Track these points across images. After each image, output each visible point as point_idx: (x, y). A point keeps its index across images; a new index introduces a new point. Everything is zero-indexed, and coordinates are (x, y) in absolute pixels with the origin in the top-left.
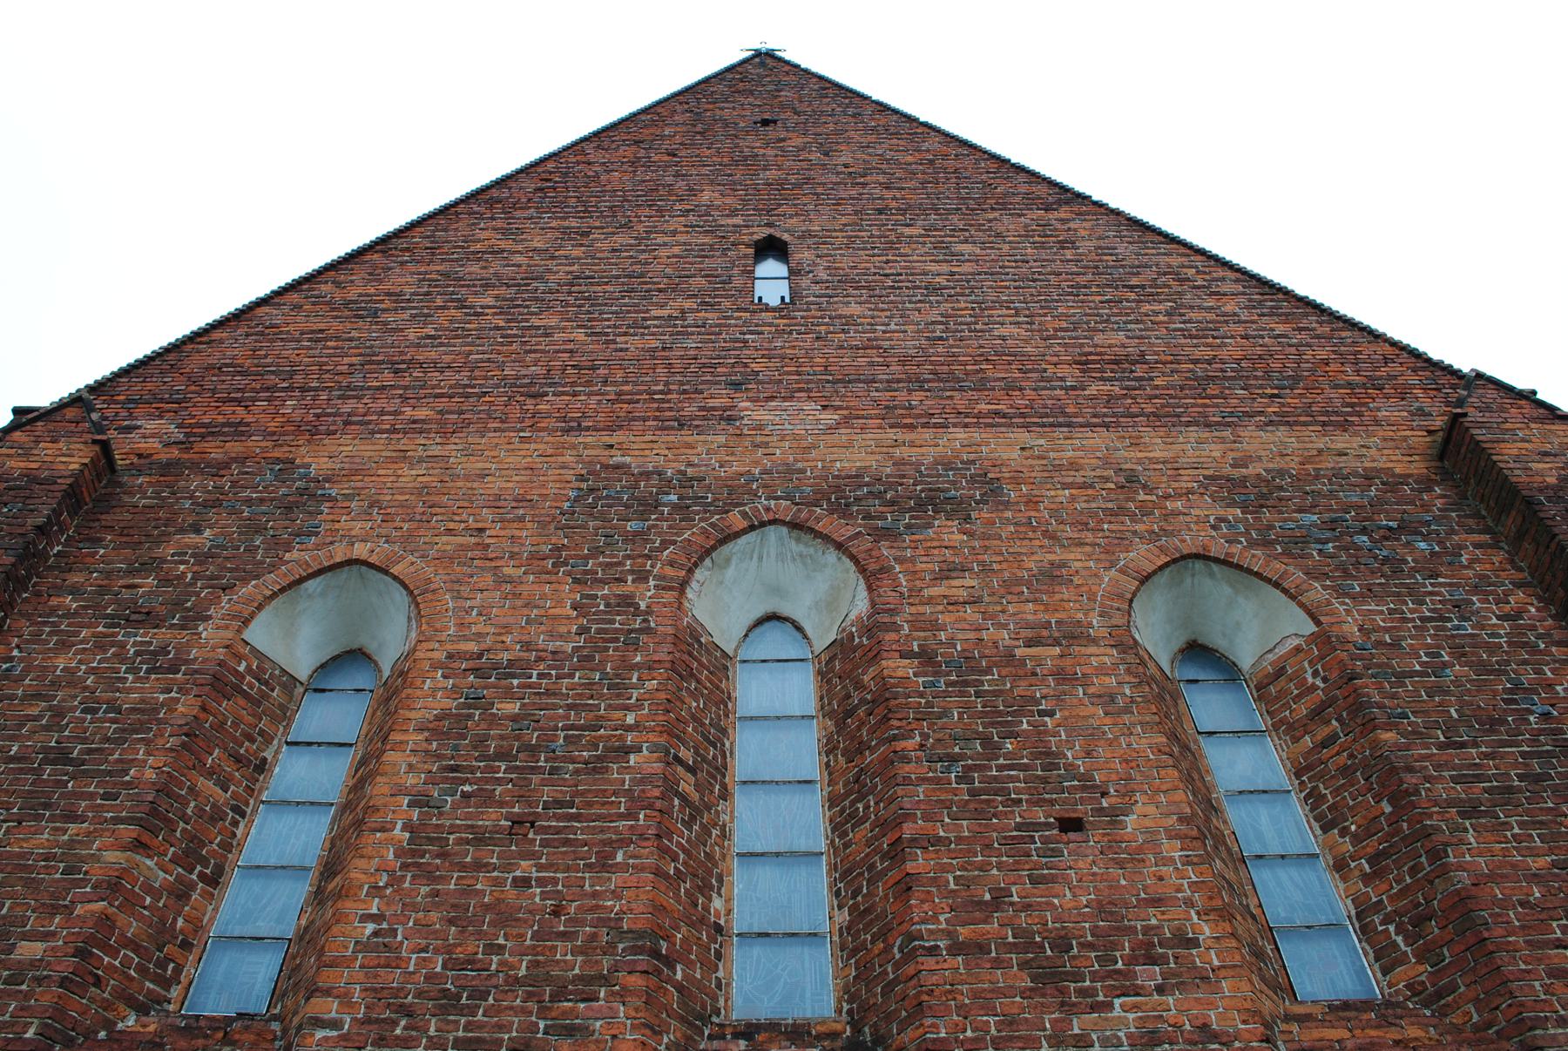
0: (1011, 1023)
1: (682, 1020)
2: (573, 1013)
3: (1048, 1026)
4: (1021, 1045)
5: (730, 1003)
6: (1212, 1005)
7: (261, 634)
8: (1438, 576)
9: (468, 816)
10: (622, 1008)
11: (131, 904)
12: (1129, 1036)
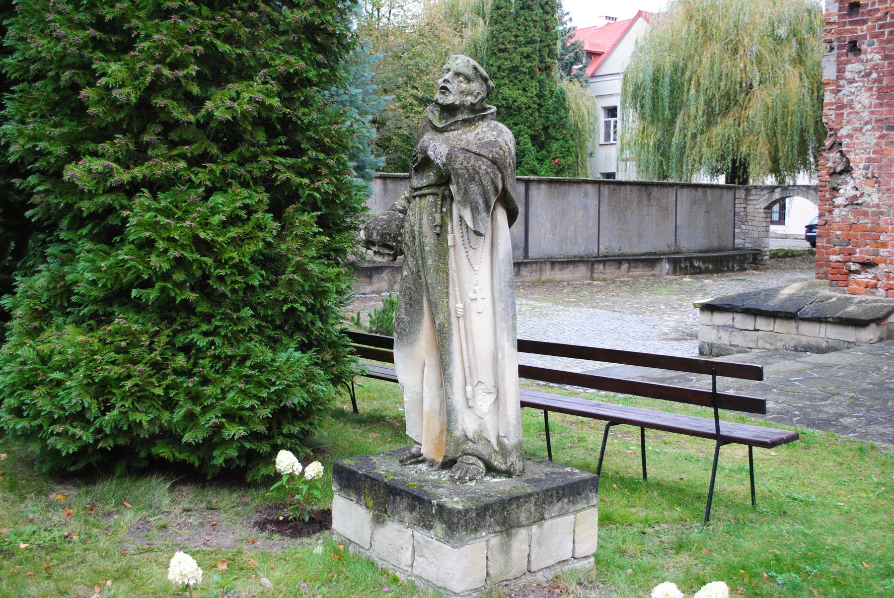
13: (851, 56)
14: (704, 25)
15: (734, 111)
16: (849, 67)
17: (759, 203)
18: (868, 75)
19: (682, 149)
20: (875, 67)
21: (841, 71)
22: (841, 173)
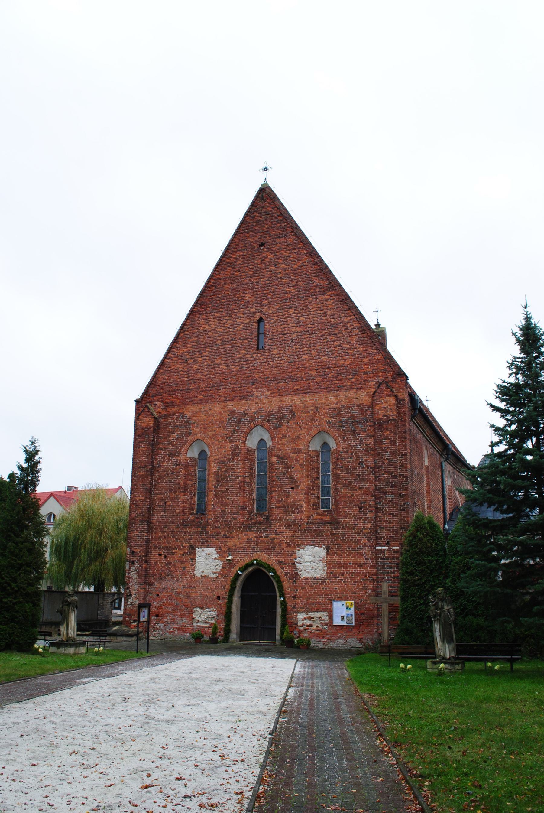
2: (235, 517)
7: (189, 455)
8: (360, 434)
9: (221, 489)
11: (186, 502)
13: (132, 565)
14: (88, 522)
15: (99, 560)
16: (132, 568)
17: (109, 600)
18: (136, 570)
19: (76, 574)
20: (138, 569)
21: (130, 568)
22: (129, 595)
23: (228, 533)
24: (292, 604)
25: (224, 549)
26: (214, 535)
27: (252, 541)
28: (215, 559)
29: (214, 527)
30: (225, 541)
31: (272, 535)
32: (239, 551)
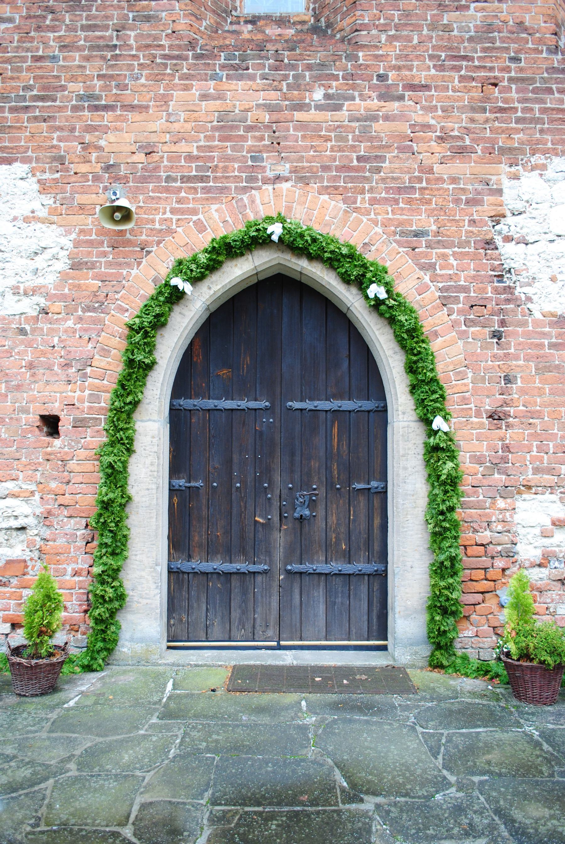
0: (407, 16)
1: (214, 11)
3: (429, 18)
4: (411, 29)
5: (243, 3)
6: (528, 10)
10: (177, 4)
12: (476, 26)
23: (106, 88)
24: (483, 449)
25: (83, 168)
26: (24, 98)
27: (249, 129)
28: (27, 220)
29: (24, 59)
30: (90, 129)
31: (363, 98)
32: (169, 179)
